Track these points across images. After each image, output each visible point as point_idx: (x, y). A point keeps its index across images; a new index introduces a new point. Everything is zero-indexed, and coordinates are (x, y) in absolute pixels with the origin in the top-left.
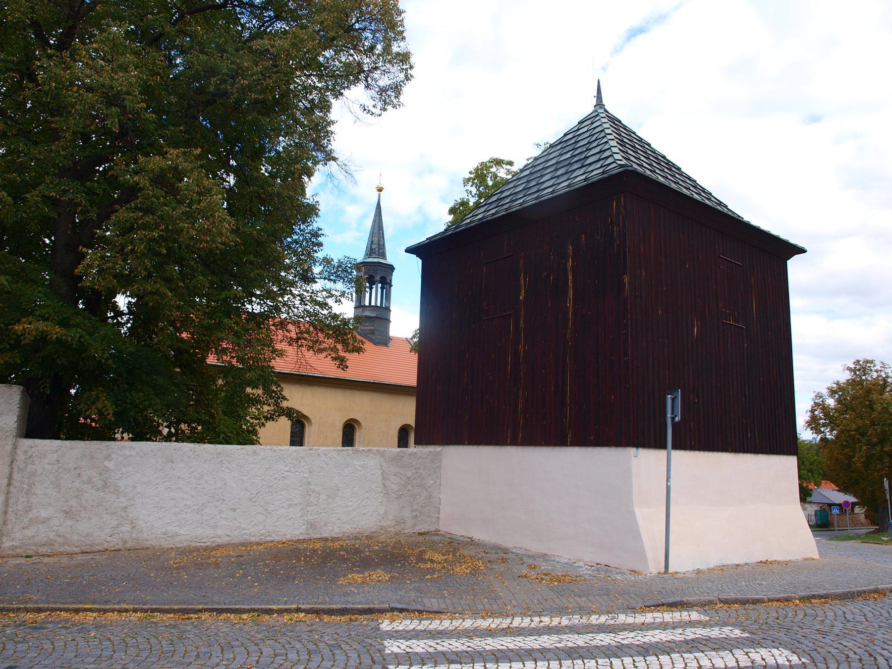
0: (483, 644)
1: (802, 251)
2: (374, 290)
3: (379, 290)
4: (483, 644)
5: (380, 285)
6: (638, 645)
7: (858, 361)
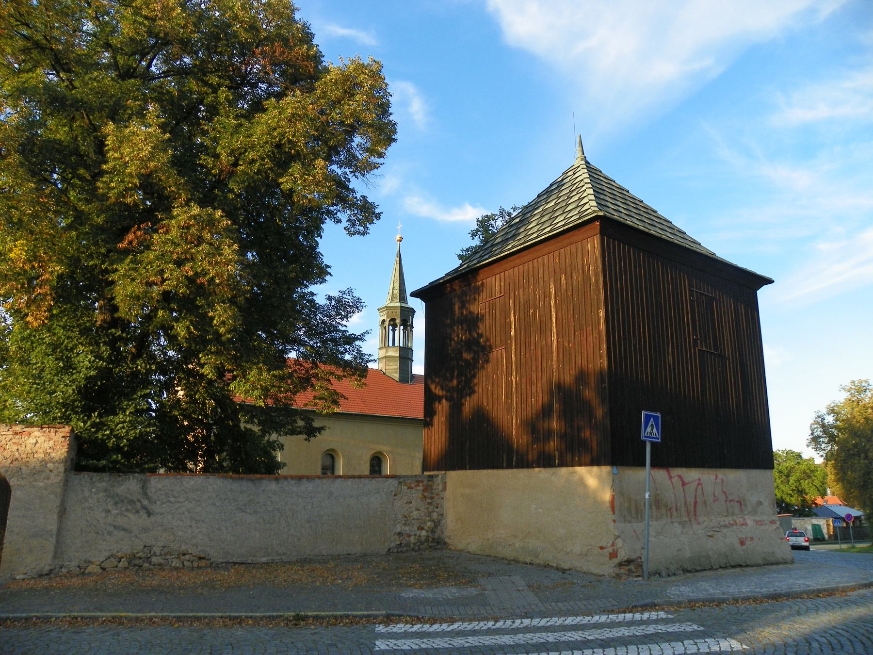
0: (817, 620)
1: (769, 281)
2: (397, 333)
3: (402, 332)
4: (817, 620)
5: (402, 327)
6: (602, 640)
7: (853, 382)
